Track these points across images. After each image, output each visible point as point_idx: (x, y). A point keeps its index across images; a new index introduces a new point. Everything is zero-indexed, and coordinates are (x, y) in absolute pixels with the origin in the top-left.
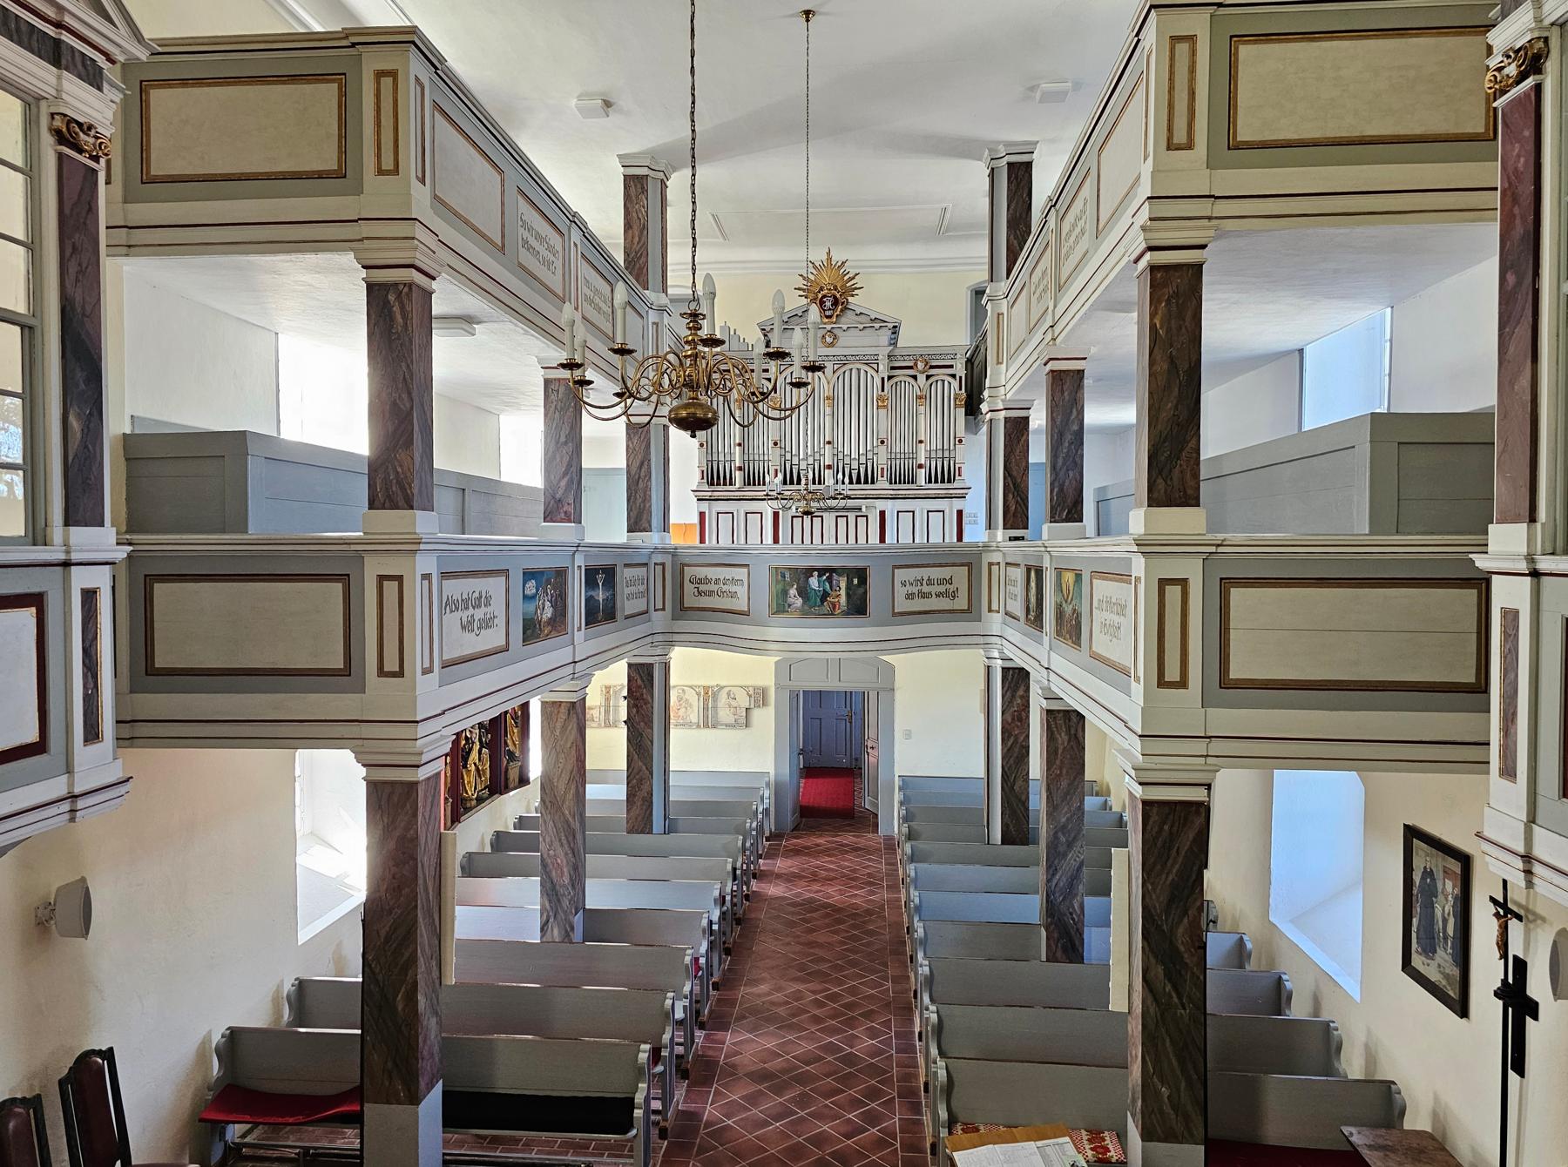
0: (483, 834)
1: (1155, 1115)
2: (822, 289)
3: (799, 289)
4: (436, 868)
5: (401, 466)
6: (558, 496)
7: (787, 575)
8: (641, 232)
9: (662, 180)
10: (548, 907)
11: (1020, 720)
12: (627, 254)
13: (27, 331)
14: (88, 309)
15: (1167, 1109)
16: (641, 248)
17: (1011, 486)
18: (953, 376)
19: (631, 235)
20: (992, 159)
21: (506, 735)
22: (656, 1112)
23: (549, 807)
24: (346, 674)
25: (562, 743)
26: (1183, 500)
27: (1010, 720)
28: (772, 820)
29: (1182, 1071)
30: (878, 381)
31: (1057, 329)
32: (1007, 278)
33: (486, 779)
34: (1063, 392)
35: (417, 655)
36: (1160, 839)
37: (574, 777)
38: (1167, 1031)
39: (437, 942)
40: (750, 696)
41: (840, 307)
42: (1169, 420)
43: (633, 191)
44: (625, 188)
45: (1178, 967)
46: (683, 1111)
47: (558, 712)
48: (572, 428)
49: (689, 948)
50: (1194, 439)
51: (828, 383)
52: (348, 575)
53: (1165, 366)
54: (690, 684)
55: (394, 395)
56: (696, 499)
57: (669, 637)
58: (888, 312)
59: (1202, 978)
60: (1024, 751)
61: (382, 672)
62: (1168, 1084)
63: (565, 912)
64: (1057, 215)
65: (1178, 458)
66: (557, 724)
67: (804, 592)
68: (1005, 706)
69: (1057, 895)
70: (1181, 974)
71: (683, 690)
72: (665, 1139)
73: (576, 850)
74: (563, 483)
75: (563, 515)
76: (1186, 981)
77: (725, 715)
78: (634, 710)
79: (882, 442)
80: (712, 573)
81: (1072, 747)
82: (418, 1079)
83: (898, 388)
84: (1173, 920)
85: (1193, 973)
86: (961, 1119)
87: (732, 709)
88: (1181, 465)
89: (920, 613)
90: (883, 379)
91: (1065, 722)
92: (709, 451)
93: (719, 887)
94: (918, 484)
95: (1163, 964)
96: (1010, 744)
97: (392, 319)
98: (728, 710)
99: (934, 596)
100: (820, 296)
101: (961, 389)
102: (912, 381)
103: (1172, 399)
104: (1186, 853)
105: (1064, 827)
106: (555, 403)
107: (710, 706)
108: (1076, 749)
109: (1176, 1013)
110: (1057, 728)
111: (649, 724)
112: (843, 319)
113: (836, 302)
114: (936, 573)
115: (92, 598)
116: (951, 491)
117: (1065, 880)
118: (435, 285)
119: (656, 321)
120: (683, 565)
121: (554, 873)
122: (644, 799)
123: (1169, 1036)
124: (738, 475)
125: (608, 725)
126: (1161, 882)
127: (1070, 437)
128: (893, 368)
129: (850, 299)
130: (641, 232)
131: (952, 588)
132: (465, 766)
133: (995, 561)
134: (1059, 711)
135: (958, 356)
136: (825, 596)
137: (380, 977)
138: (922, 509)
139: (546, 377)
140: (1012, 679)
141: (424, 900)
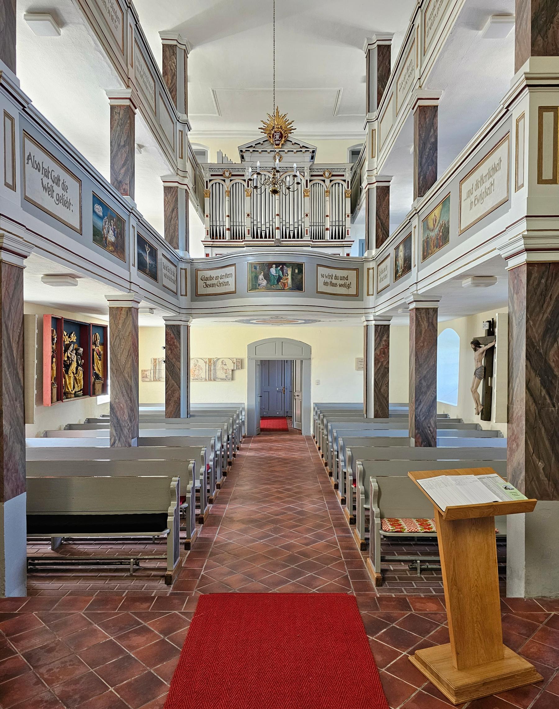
0: (80, 420)
1: (534, 481)
3: (261, 128)
6: (119, 179)
7: (258, 268)
8: (173, 78)
9: (186, 190)
10: (115, 435)
11: (384, 353)
15: (542, 476)
16: (173, 86)
17: (380, 225)
18: (345, 181)
20: (369, 45)
21: (93, 363)
22: (183, 530)
23: (115, 372)
25: (123, 333)
27: (379, 354)
28: (246, 430)
29: (553, 450)
31: (422, 80)
33: (81, 385)
34: (425, 118)
37: (131, 354)
38: (542, 423)
39: (21, 391)
40: (234, 363)
41: (283, 139)
43: (168, 53)
45: (550, 378)
46: (200, 538)
47: (121, 314)
48: (128, 136)
49: (204, 447)
54: (230, 357)
58: (311, 143)
60: (386, 370)
62: (544, 461)
63: (125, 437)
64: (422, 14)
65: (552, 23)
66: (120, 321)
67: (267, 277)
68: (376, 346)
69: (421, 416)
70: (551, 382)
71: (197, 361)
72: (189, 550)
73: (132, 399)
74: (123, 171)
77: (220, 374)
80: (213, 273)
81: (430, 330)
82: (3, 483)
83: (315, 187)
84: (547, 345)
86: (386, 517)
87: (224, 371)
88: (553, 27)
90: (307, 181)
91: (426, 315)
92: (211, 220)
93: (220, 431)
94: (326, 239)
95: (540, 376)
96: (379, 366)
98: (222, 371)
99: (338, 286)
101: (348, 188)
102: (322, 183)
105: (425, 377)
106: (117, 121)
108: (432, 331)
109: (548, 410)
110: (422, 319)
111: (178, 359)
112: (285, 147)
113: (281, 137)
116: (344, 243)
117: (425, 408)
119: (181, 130)
120: (197, 270)
121: (118, 413)
122: (175, 402)
124: (227, 234)
125: (155, 380)
127: (429, 146)
128: (312, 176)
131: (348, 282)
132: (67, 372)
133: (371, 267)
134: (422, 309)
135: (347, 170)
136: (279, 279)
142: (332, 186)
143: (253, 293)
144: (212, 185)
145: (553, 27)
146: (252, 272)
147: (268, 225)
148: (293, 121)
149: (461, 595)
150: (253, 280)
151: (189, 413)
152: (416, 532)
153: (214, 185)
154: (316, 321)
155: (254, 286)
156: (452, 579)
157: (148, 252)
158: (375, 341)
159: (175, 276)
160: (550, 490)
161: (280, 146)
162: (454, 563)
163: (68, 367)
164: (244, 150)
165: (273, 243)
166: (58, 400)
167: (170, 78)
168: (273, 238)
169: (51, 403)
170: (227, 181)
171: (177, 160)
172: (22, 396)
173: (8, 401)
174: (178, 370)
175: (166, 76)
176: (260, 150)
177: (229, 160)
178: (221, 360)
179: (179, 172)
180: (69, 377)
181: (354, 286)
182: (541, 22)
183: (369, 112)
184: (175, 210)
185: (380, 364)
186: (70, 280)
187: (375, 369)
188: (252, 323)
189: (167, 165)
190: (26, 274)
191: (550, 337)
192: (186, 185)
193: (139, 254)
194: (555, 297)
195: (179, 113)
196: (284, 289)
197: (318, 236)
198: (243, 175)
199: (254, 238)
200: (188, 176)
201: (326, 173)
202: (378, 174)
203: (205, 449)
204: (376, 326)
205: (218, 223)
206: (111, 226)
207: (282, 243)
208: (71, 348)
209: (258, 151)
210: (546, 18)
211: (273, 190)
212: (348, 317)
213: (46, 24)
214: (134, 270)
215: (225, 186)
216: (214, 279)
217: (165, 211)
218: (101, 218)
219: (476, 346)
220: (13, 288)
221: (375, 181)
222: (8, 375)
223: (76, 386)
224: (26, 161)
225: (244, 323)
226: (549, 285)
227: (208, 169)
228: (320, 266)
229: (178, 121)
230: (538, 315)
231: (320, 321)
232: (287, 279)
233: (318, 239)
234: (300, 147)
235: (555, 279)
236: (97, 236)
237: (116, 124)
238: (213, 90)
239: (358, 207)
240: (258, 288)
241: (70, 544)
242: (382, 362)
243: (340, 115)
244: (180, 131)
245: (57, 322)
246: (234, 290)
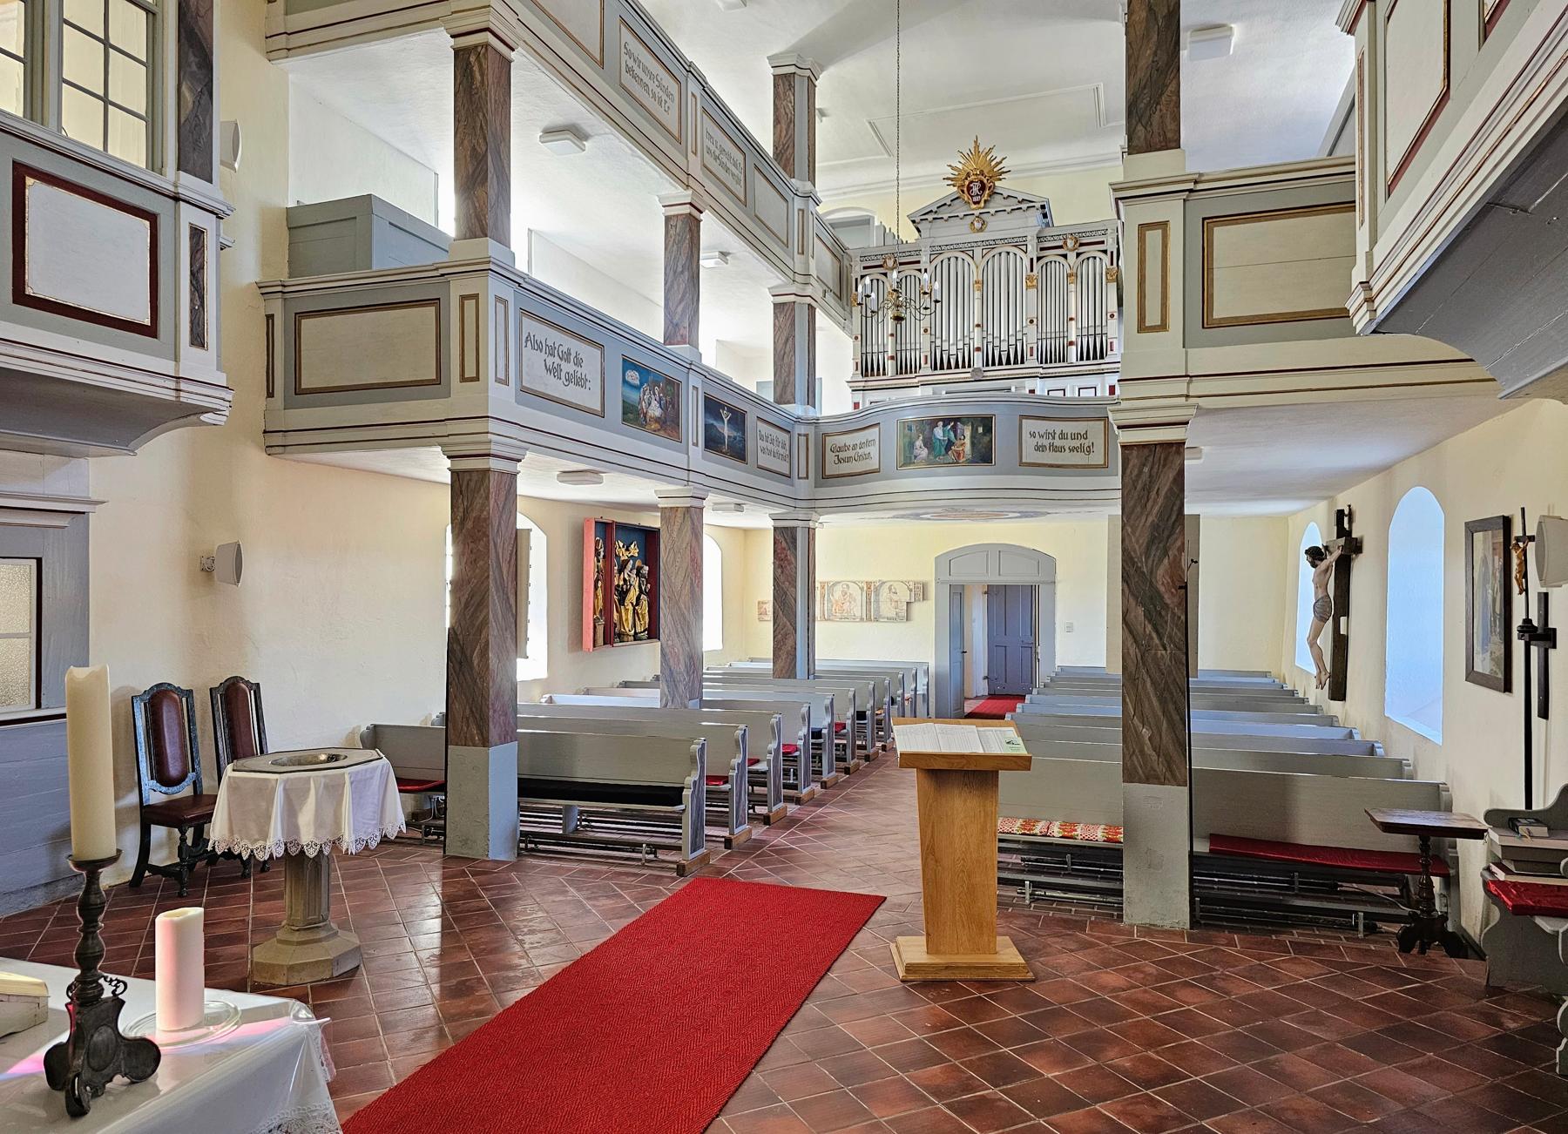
2: (968, 175)
3: (948, 179)
4: (511, 555)
5: (478, 201)
6: (675, 321)
7: (914, 428)
9: (809, 77)
12: (775, 147)
13: (150, 15)
14: (202, 12)
18: (1105, 252)
19: (779, 129)
24: (436, 384)
26: (1163, 144)
29: (1164, 712)
30: (1027, 262)
35: (490, 371)
36: (1140, 482)
39: (512, 620)
40: (911, 590)
41: (987, 192)
42: (1147, 68)
44: (775, 87)
50: (1174, 82)
51: (977, 267)
52: (439, 299)
53: (1144, 14)
54: (855, 580)
55: (473, 141)
56: (850, 390)
57: (811, 504)
58: (1040, 190)
59: (1183, 617)
61: (463, 379)
63: (681, 696)
65: (1158, 104)
66: (675, 527)
67: (929, 443)
70: (1160, 613)
71: (847, 585)
74: (680, 309)
75: (679, 338)
76: (1166, 622)
77: (887, 609)
78: (780, 571)
79: (1032, 322)
84: (1153, 561)
85: (1174, 614)
87: (893, 603)
88: (1161, 110)
90: (1032, 260)
97: (473, 78)
99: (1067, 450)
100: (967, 183)
101: (1112, 264)
103: (1150, 45)
104: (1166, 493)
109: (1156, 654)
112: (991, 204)
113: (983, 188)
114: (1070, 428)
115: (200, 237)
118: (513, 55)
119: (802, 208)
120: (825, 435)
121: (671, 660)
123: (1150, 677)
124: (890, 365)
126: (1141, 524)
128: (1042, 249)
129: (997, 183)
130: (789, 126)
131: (1087, 443)
135: (1109, 231)
136: (950, 444)
137: (460, 637)
138: (1073, 387)
139: (667, 214)
141: (496, 573)
145: (1161, 110)
147: (960, 345)
149: (939, 868)
151: (811, 672)
152: (1010, 833)
155: (908, 459)
156: (928, 846)
157: (726, 420)
159: (788, 449)
160: (1161, 769)
161: (982, 204)
162: (933, 827)
163: (623, 594)
164: (917, 220)
165: (969, 375)
166: (605, 644)
167: (784, 127)
169: (594, 646)
172: (513, 626)
173: (496, 631)
175: (779, 126)
176: (945, 217)
178: (888, 585)
179: (798, 278)
180: (627, 610)
182: (1142, 105)
186: (589, 476)
189: (772, 272)
190: (519, 479)
191: (1157, 549)
193: (708, 427)
194: (1164, 493)
197: (1053, 357)
198: (918, 262)
201: (1069, 241)
203: (778, 716)
206: (654, 394)
207: (986, 374)
208: (630, 566)
209: (942, 218)
210: (1151, 99)
213: (565, 144)
214: (697, 452)
217: (774, 342)
218: (637, 388)
219: (1314, 558)
220: (503, 499)
222: (497, 601)
223: (638, 622)
224: (524, 344)
226: (1155, 474)
227: (858, 259)
230: (1139, 517)
233: (1055, 362)
234: (1019, 202)
235: (1164, 466)
236: (629, 414)
237: (671, 243)
241: (587, 831)
243: (1114, 124)
245: (607, 530)
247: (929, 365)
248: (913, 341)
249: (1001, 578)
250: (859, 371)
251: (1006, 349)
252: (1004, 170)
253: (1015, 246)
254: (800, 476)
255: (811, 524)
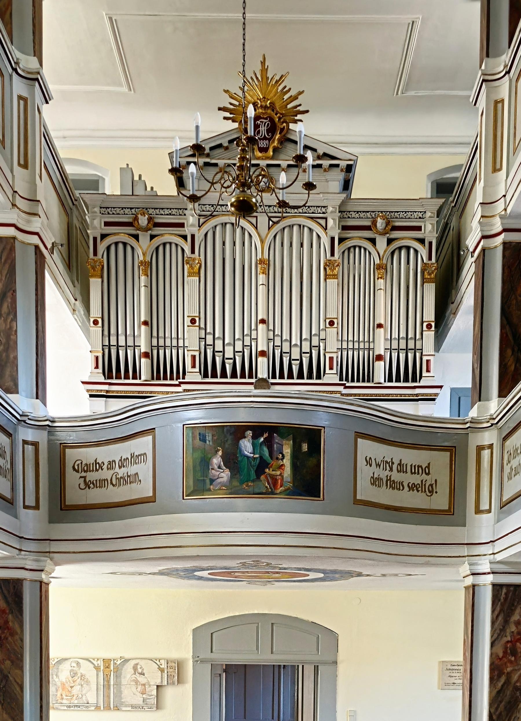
7: (209, 438)
9: (37, 247)
27: (501, 655)
30: (325, 241)
32: (509, 47)
40: (162, 671)
68: (496, 636)
71: (78, 664)
83: (352, 255)
87: (140, 687)
89: (388, 508)
90: (333, 239)
92: (106, 333)
94: (376, 380)
96: (500, 684)
98: (134, 688)
99: (406, 488)
101: (430, 258)
102: (368, 245)
107: (112, 683)
112: (282, 156)
113: (272, 129)
119: (25, 94)
120: (64, 446)
124: (144, 364)
128: (345, 228)
129: (292, 126)
131: (429, 480)
133: (487, 443)
135: (428, 214)
140: (506, 599)
142: (393, 253)
143: (193, 501)
144: (108, 248)
146: (194, 449)
148: (300, 93)
150: (198, 468)
153: (113, 248)
154: (350, 574)
158: (493, 623)
159: (8, 458)
168: (251, 377)
170: (144, 238)
171: (12, 171)
174: (18, 689)
176: (221, 163)
177: (149, 189)
178: (132, 663)
179: (19, 202)
181: (443, 489)
183: (488, 56)
184: (9, 294)
185: (503, 679)
187: (490, 692)
188: (201, 578)
192: (37, 234)
195: (16, 52)
196: (273, 493)
199: (206, 376)
200: (41, 213)
202: (509, 210)
204: (497, 587)
205: (122, 339)
211: (238, 201)
212: (427, 564)
215: (139, 252)
216: (105, 467)
221: (500, 229)
225: (181, 577)
227: (97, 210)
228: (362, 438)
229: (15, 70)
231: (360, 575)
232: (281, 467)
238: (111, 19)
239: (452, 307)
240: (209, 490)
242: (509, 675)
243: (412, 93)
244: (20, 97)
246: (151, 494)
247: (197, 369)
248: (174, 335)
249: (274, 657)
250: (100, 370)
251: (298, 357)
252: (300, 108)
253: (312, 218)
254: (27, 504)
255: (44, 576)
